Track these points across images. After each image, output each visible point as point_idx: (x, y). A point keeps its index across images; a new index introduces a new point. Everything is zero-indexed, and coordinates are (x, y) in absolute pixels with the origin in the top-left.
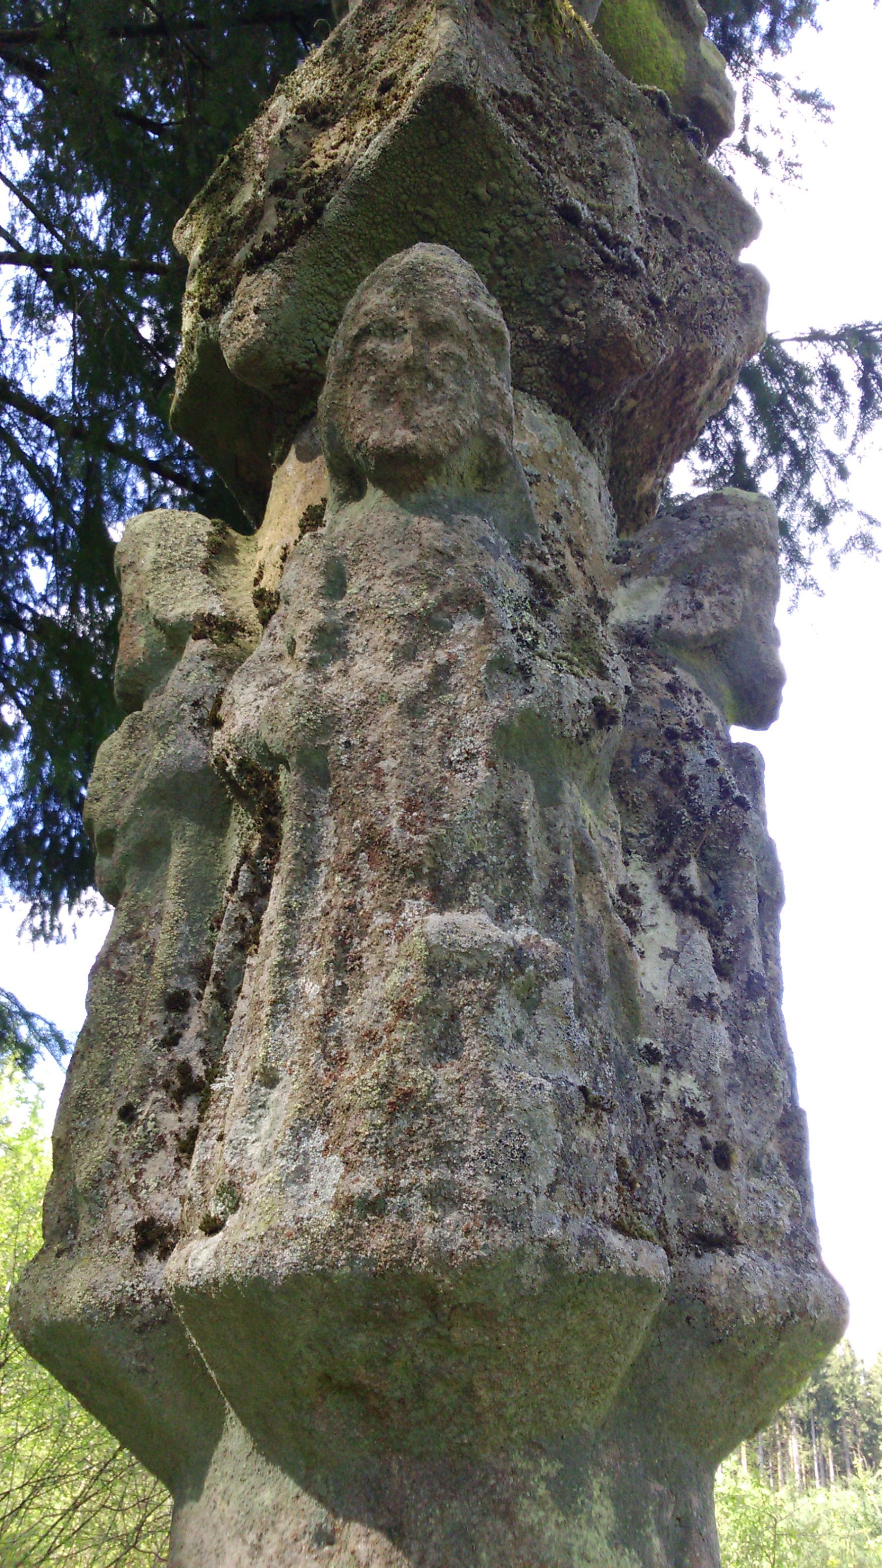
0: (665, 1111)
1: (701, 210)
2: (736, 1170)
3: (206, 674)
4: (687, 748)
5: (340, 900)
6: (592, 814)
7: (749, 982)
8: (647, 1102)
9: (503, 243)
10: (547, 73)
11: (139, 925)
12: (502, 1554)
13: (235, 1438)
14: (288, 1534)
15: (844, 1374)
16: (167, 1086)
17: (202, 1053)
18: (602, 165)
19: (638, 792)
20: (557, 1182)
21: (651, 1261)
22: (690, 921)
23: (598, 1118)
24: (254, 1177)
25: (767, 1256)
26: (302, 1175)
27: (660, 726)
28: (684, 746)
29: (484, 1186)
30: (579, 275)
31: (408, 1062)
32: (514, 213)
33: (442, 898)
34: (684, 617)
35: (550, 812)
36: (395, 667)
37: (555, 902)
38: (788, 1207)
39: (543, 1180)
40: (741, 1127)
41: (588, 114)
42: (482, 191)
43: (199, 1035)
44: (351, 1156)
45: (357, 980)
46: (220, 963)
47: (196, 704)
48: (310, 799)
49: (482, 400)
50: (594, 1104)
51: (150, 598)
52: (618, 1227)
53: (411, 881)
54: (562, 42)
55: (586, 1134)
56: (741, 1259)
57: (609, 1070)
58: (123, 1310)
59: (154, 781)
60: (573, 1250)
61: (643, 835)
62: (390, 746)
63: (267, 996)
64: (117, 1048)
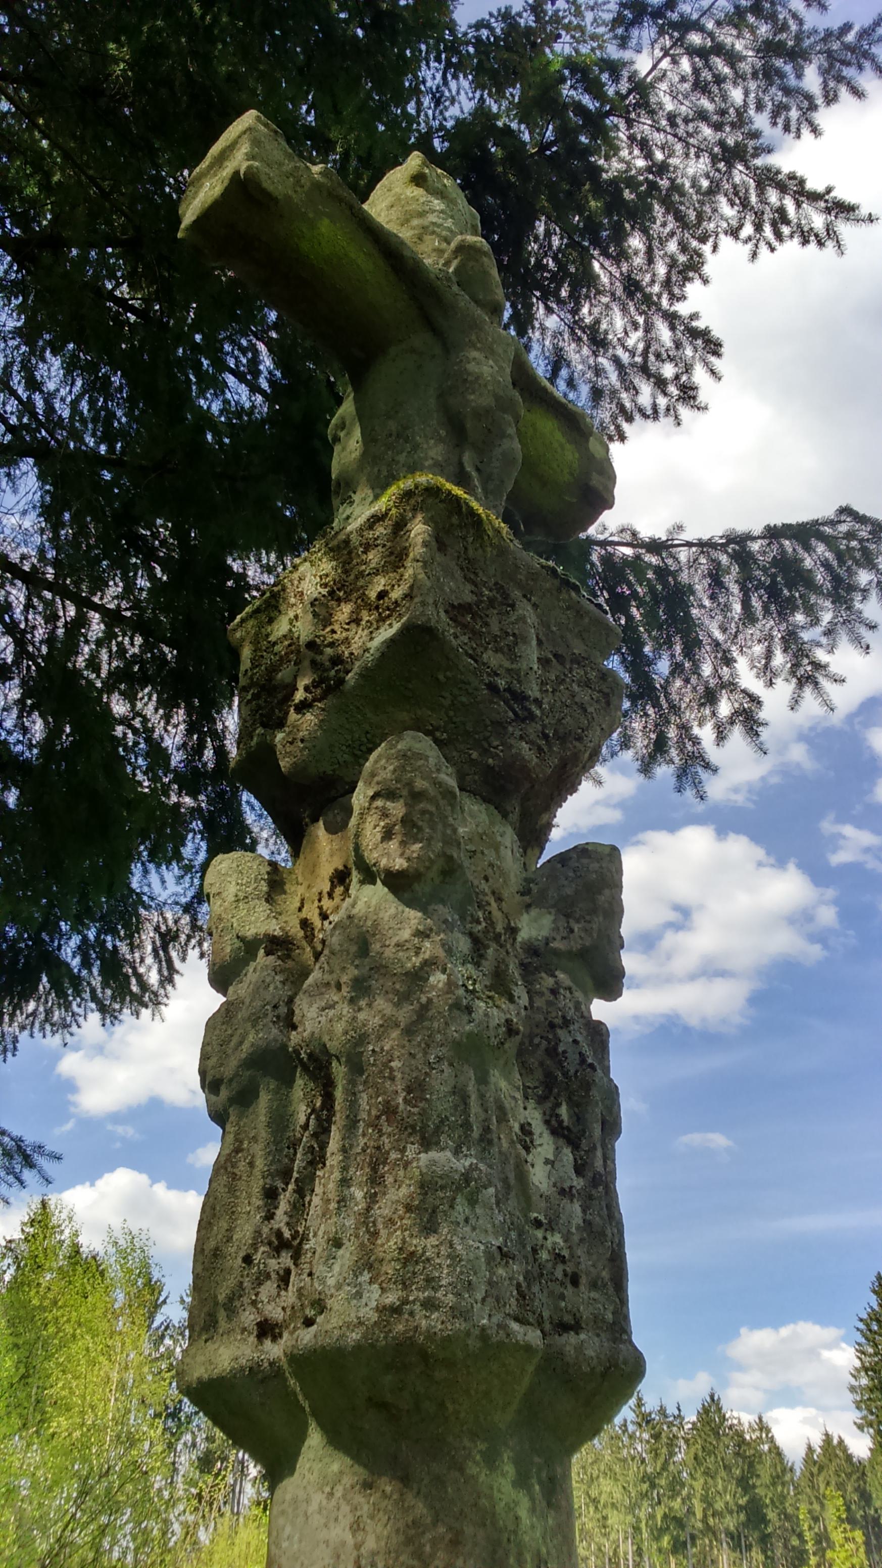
0: (544, 1255)
1: (580, 635)
2: (582, 1288)
3: (280, 986)
4: (561, 1033)
5: (372, 1143)
6: (505, 1084)
7: (594, 1178)
8: (535, 1251)
9: (453, 704)
10: (481, 574)
11: (241, 1142)
12: (459, 1489)
13: (315, 1439)
14: (348, 1486)
15: (774, 1484)
16: (270, 1244)
17: (288, 1224)
18: (514, 635)
19: (533, 1061)
20: (486, 1296)
21: (533, 1336)
22: (561, 1142)
23: (507, 1262)
24: (332, 1296)
25: (598, 1335)
26: (359, 1295)
27: (546, 1019)
28: (559, 1032)
29: (450, 1299)
30: (500, 726)
31: (411, 1236)
32: (460, 689)
33: (427, 1144)
34: (563, 938)
35: (483, 1087)
36: (398, 1005)
37: (486, 1140)
38: (611, 1308)
39: (479, 1296)
40: (586, 1263)
41: (506, 596)
42: (441, 677)
43: (286, 1213)
44: (384, 1285)
45: (382, 1189)
46: (298, 1172)
47: (275, 1007)
48: (352, 1082)
49: (444, 834)
50: (505, 1255)
51: (234, 920)
52: (517, 1319)
53: (411, 1134)
54: (489, 549)
55: (501, 1271)
56: (583, 1336)
57: (513, 1235)
58: (254, 1370)
59: (251, 1054)
60: (494, 1332)
61: (536, 1088)
62: (397, 1053)
63: (333, 1195)
64: (236, 1219)
